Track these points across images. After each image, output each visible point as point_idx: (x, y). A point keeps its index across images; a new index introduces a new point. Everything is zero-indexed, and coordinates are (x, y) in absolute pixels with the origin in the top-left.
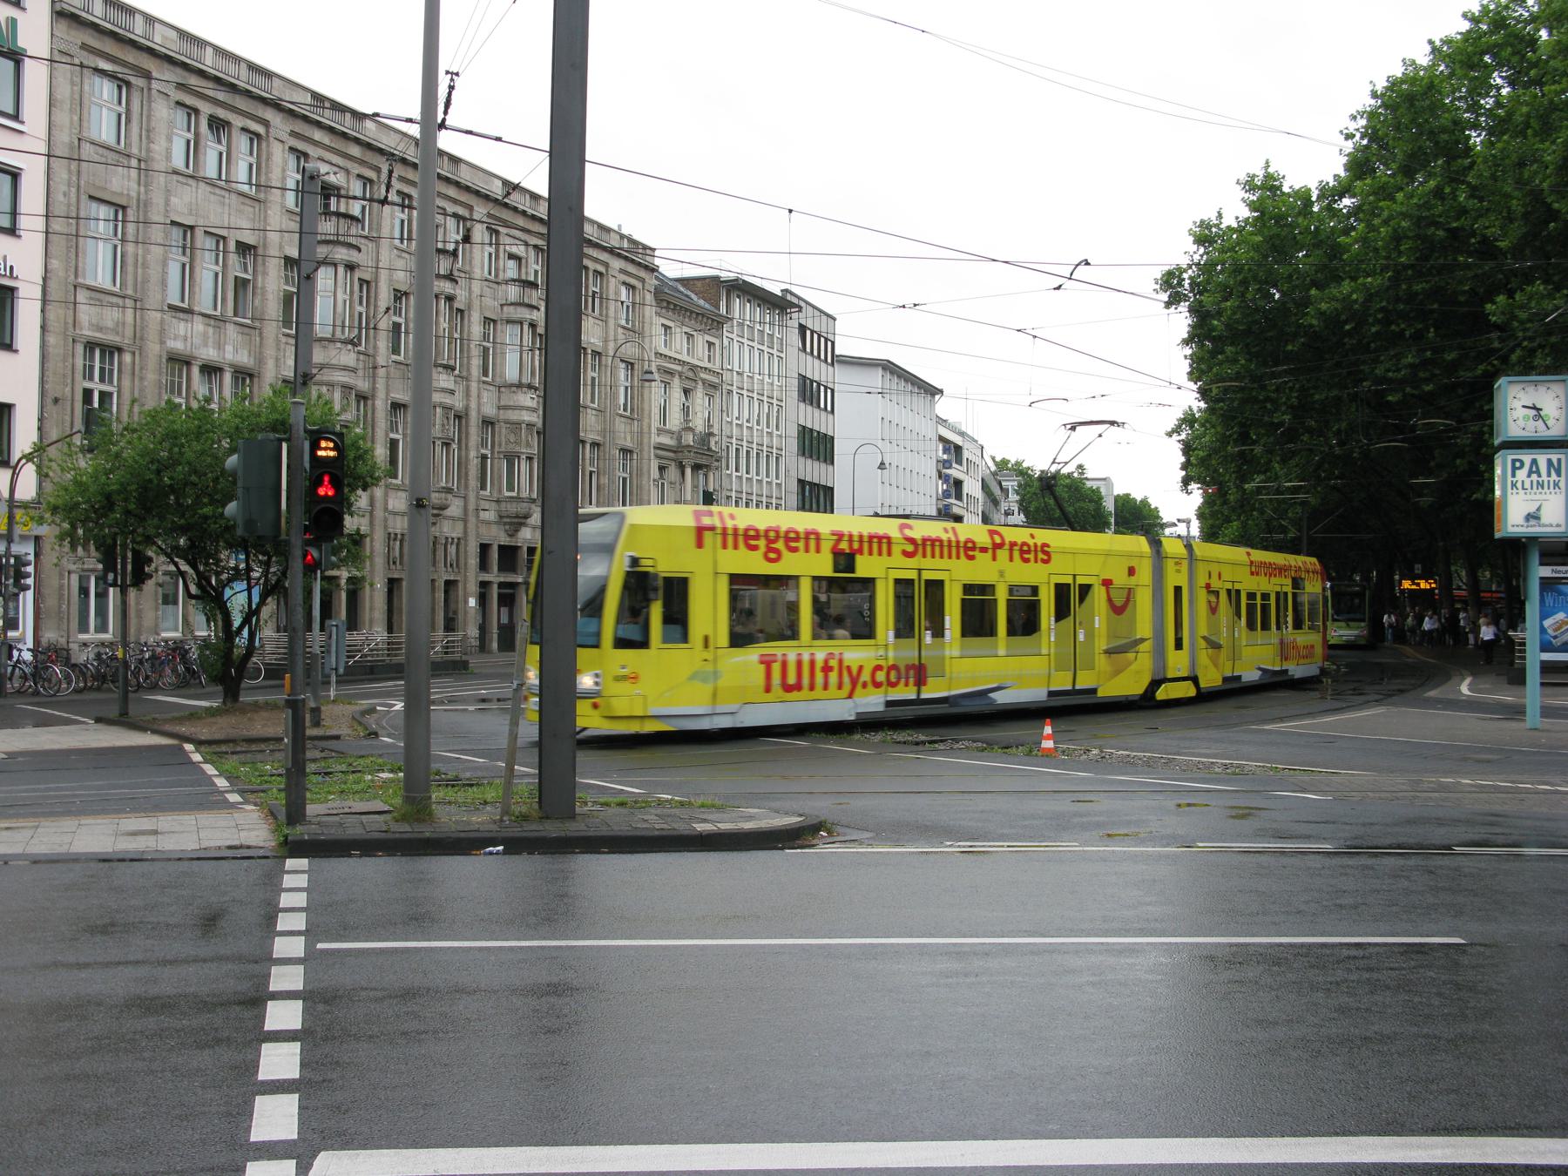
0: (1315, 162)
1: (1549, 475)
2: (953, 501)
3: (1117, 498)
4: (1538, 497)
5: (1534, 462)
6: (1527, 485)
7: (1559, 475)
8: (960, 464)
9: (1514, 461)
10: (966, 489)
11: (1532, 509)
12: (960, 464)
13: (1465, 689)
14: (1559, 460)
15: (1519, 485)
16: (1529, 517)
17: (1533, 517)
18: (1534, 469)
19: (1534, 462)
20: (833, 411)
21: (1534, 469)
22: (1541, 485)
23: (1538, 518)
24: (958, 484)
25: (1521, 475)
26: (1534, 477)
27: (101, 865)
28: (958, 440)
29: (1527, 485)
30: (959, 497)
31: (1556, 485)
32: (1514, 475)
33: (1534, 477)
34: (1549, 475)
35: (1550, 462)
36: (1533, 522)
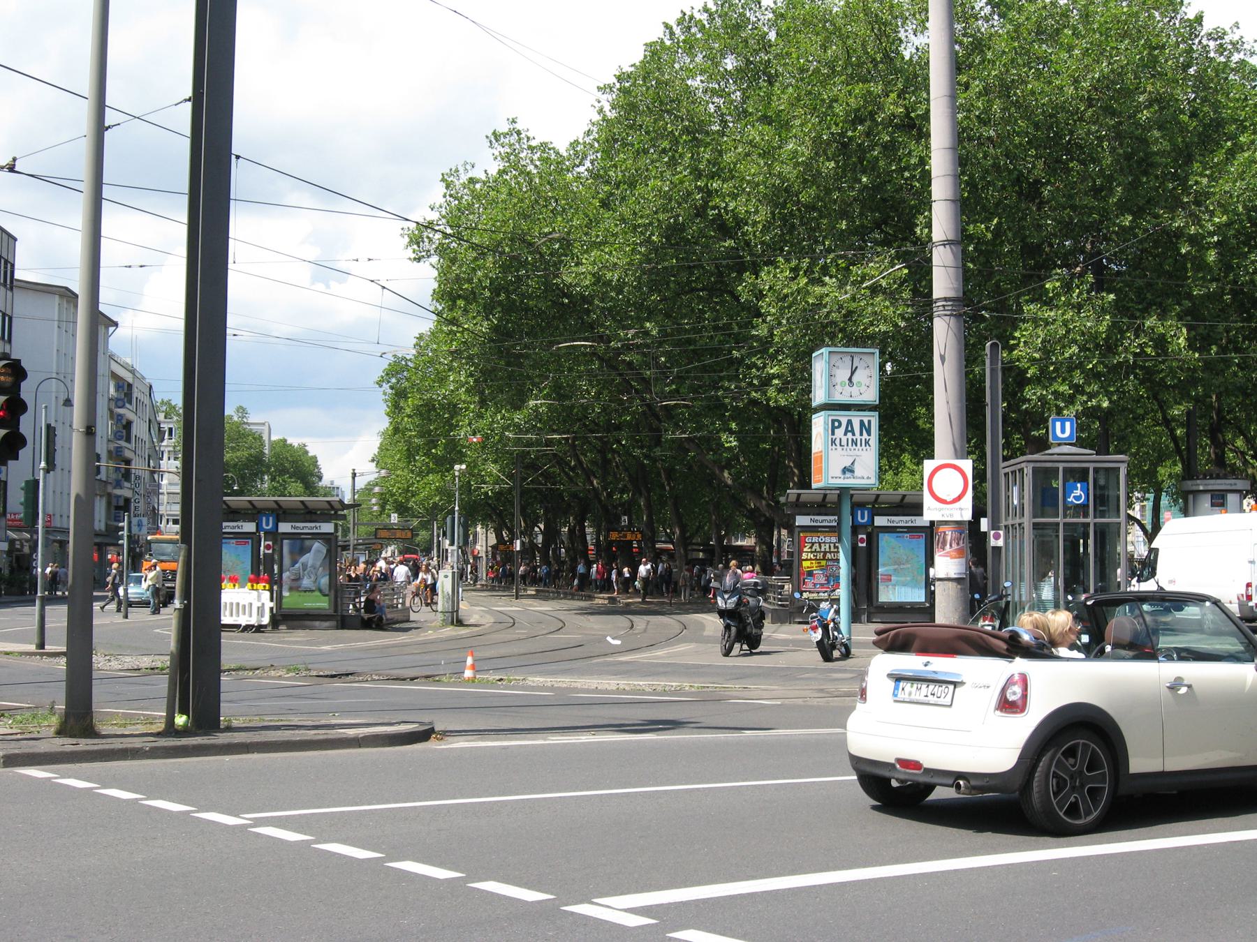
0: (565, 115)
1: (861, 434)
2: (123, 443)
3: (273, 445)
4: (852, 453)
5: (850, 422)
6: (844, 442)
7: (869, 434)
8: (130, 403)
9: (833, 421)
10: (135, 430)
11: (848, 464)
12: (130, 403)
13: (1007, 584)
14: (869, 422)
15: (837, 442)
16: (845, 470)
17: (848, 470)
18: (849, 429)
19: (850, 422)
20: (10, 341)
21: (849, 429)
22: (854, 442)
23: (852, 471)
24: (128, 425)
25: (840, 432)
26: (849, 435)
27: (351, 669)
28: (128, 377)
29: (844, 442)
30: (128, 440)
31: (867, 443)
32: (833, 433)
33: (849, 435)
34: (861, 434)
35: (862, 423)
36: (848, 474)
